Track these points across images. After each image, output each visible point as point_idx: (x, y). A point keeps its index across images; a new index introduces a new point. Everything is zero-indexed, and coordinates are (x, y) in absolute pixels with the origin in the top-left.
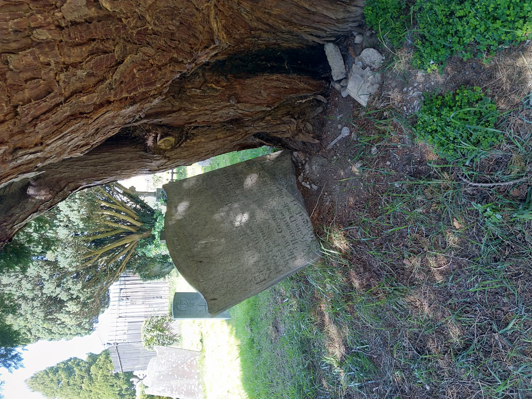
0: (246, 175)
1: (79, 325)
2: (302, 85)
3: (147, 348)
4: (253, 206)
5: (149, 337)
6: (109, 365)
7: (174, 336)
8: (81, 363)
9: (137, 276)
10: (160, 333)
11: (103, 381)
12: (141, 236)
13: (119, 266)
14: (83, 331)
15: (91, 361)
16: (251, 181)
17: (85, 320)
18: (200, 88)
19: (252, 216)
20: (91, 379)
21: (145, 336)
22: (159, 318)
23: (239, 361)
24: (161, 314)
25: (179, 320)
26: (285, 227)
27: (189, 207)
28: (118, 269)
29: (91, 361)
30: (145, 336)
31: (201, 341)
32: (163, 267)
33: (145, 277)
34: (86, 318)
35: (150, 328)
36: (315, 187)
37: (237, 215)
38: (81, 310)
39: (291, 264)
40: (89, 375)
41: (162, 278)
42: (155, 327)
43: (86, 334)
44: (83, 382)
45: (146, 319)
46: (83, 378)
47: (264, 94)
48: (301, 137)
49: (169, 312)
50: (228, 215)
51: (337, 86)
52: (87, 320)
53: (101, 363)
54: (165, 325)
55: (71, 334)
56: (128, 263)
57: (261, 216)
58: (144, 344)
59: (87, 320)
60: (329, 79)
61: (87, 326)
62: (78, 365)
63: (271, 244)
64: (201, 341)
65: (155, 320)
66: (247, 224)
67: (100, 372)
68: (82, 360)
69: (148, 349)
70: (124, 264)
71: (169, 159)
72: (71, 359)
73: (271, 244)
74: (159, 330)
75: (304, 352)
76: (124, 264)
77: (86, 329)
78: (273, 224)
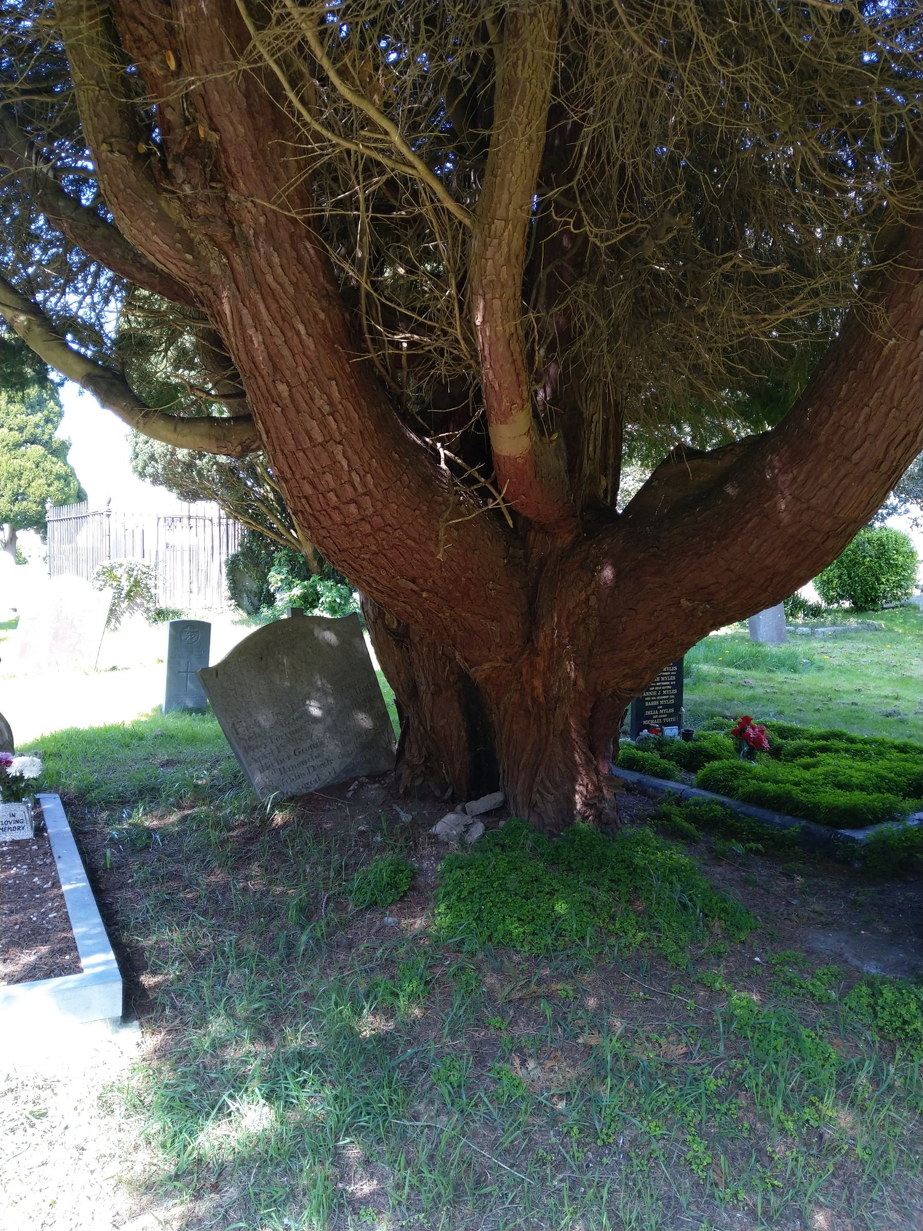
0: (368, 712)
1: (152, 457)
2: (458, 766)
3: (98, 568)
4: (329, 721)
5: (119, 572)
6: (43, 481)
7: (117, 619)
8: (50, 426)
9: (234, 549)
10: (124, 592)
11: (11, 470)
12: (311, 557)
13: (255, 521)
14: (141, 464)
15: (54, 446)
16: (364, 721)
17: (160, 466)
18: (443, 653)
19: (315, 720)
20: (17, 445)
21: (121, 565)
22: (153, 591)
23: (102, 725)
24: (159, 592)
25: (822, 730)
26: (301, 759)
27: (328, 644)
28: (251, 517)
29: (54, 446)
30: (121, 565)
31: (114, 668)
32: (251, 596)
33: (233, 562)
34: (164, 468)
35: (135, 573)
36: (349, 794)
37: (318, 701)
38: (179, 461)
39: (255, 766)
40: (26, 442)
41: (229, 594)
42: (137, 583)
43: (135, 468)
44: (11, 430)
45: (153, 566)
46: (21, 429)
47: (443, 722)
48: (406, 773)
49: (164, 607)
50: (318, 690)
51: (459, 808)
52: (160, 471)
53: (47, 465)
54: (139, 601)
55: (137, 444)
56: (261, 534)
57: (318, 731)
58: (107, 563)
59: (160, 471)
60: (469, 799)
61: (149, 470)
62: (48, 421)
63: (281, 741)
64: (114, 668)
65: (151, 583)
66: (307, 713)
67: (29, 465)
68: (56, 428)
69: (95, 571)
70: (260, 528)
71: (375, 623)
72: (61, 406)
73: (281, 741)
74: (130, 591)
75: (141, 793)
76: (260, 528)
77: (144, 468)
78: (306, 745)
